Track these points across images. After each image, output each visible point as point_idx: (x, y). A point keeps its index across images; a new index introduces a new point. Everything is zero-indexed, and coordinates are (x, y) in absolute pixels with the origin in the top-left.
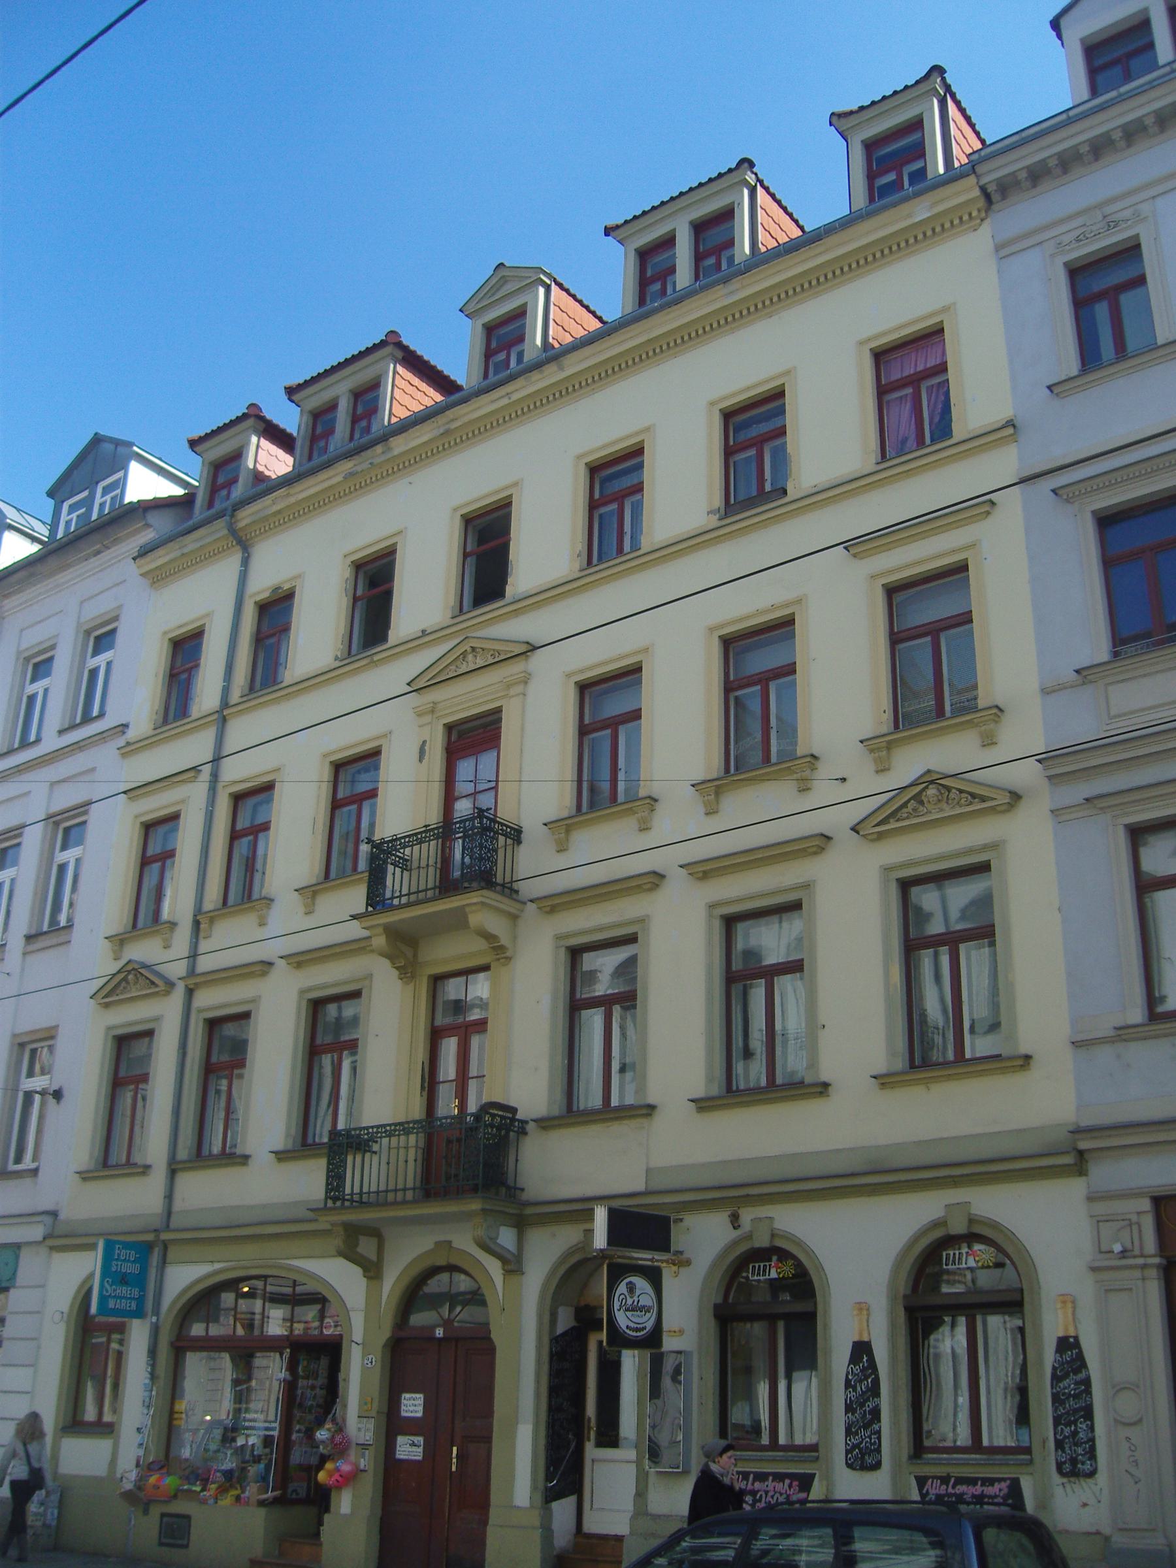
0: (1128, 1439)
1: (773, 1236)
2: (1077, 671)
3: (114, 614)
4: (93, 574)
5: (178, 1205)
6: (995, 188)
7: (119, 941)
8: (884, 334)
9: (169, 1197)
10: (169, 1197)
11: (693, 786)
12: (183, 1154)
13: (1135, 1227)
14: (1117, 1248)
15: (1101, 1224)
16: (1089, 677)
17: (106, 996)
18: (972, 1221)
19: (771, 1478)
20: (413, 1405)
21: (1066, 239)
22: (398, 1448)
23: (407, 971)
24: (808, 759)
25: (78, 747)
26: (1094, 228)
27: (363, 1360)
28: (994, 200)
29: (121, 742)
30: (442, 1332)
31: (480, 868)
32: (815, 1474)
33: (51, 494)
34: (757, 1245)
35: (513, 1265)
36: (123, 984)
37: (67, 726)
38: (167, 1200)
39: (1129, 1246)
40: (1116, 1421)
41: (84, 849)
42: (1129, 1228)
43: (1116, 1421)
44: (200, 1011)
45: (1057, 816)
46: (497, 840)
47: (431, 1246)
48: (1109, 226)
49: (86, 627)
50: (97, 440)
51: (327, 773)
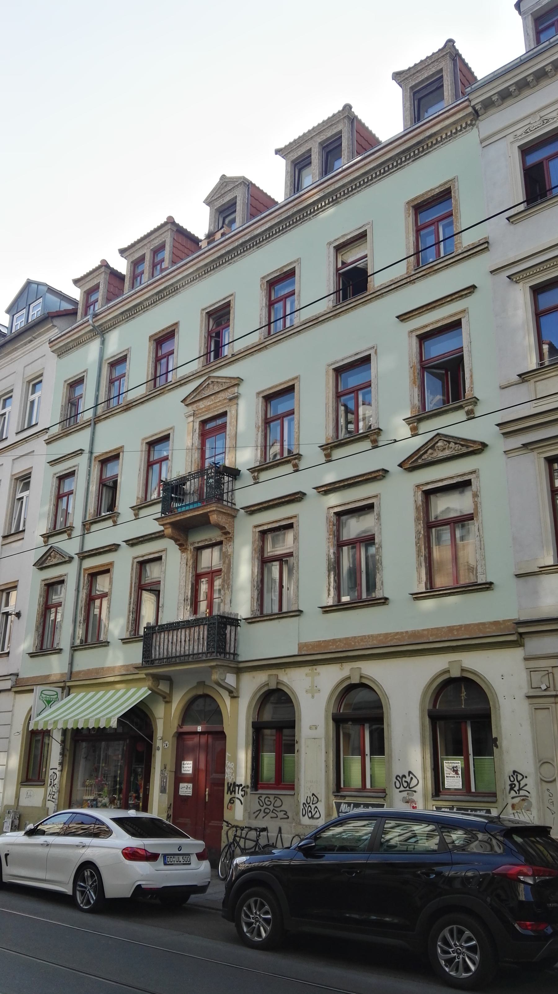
0: (548, 790)
1: (361, 677)
2: (518, 375)
3: (40, 373)
4: (30, 352)
5: (76, 669)
6: (480, 106)
7: (47, 537)
8: (277, 386)
9: (71, 664)
10: (71, 664)
11: (319, 447)
12: (78, 642)
13: (551, 675)
14: (544, 687)
15: (532, 672)
16: (525, 379)
17: (40, 565)
18: (463, 670)
19: (362, 806)
20: (188, 767)
21: (519, 133)
22: (180, 790)
23: (182, 547)
24: (377, 431)
25: (25, 440)
26: (535, 124)
27: (163, 745)
28: (480, 114)
29: (46, 437)
30: (200, 729)
31: (215, 493)
32: (384, 804)
33: (8, 311)
34: (353, 682)
35: (234, 694)
36: (49, 558)
37: (20, 430)
38: (70, 665)
39: (548, 685)
40: (541, 779)
41: (30, 492)
42: (547, 675)
43: (541, 779)
44: (85, 570)
45: (507, 454)
46: (224, 478)
47: (195, 684)
48: (544, 122)
49: (28, 379)
50: (29, 283)
51: (144, 447)
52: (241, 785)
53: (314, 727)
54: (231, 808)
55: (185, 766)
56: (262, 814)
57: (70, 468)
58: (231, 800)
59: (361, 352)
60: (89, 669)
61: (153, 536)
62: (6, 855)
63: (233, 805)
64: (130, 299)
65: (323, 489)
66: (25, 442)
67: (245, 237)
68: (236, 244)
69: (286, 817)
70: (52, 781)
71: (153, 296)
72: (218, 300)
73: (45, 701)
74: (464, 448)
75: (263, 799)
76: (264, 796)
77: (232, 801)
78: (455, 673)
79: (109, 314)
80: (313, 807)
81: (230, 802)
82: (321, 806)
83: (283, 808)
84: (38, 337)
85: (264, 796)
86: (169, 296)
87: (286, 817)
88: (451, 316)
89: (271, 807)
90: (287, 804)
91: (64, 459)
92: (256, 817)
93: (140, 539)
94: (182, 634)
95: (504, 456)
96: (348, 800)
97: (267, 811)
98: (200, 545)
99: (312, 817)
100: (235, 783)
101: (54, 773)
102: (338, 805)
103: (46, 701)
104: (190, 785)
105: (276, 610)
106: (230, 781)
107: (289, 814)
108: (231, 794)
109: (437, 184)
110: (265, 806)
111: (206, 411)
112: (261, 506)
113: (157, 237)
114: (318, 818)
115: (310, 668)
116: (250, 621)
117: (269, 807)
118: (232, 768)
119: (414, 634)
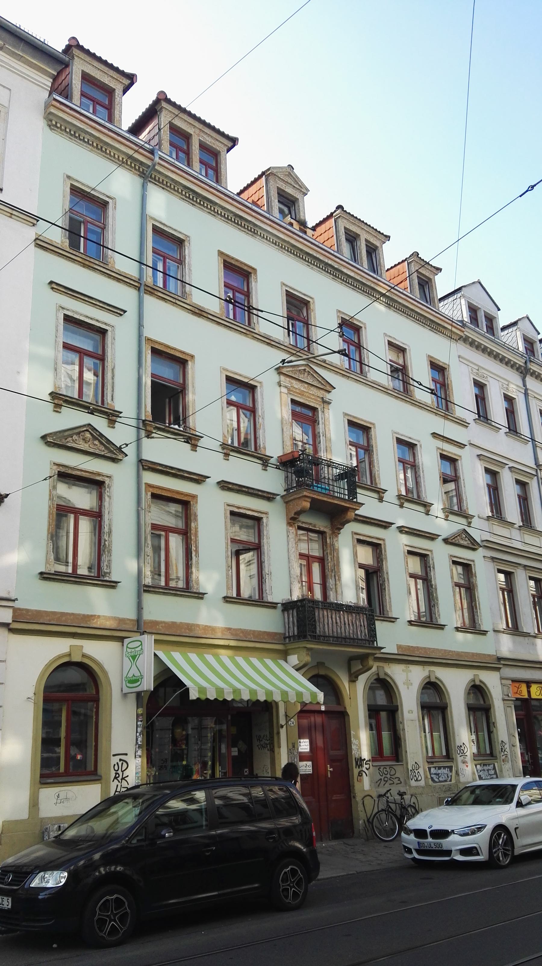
18: (84, 656)
52: (365, 759)
53: (411, 712)
54: (361, 779)
55: (301, 744)
56: (383, 782)
57: (97, 321)
58: (359, 773)
59: (413, 439)
60: (175, 623)
61: (260, 493)
62: (516, 829)
63: (361, 778)
64: (230, 201)
65: (407, 530)
66: (9, 215)
67: (336, 264)
68: (326, 260)
69: (399, 782)
70: (120, 772)
71: (232, 212)
72: (299, 290)
73: (130, 658)
74: (106, 451)
75: (381, 770)
76: (382, 768)
77: (360, 774)
78: (77, 658)
79: (173, 171)
80: (416, 772)
81: (359, 775)
82: (421, 771)
83: (396, 776)
84: (5, 52)
85: (382, 768)
86: (244, 230)
87: (399, 782)
88: (455, 454)
89: (388, 776)
90: (399, 772)
91: (86, 299)
92: (379, 785)
93: (244, 489)
94: (346, 617)
95: (483, 558)
96: (435, 765)
97: (386, 779)
98: (304, 525)
99: (417, 780)
100: (361, 758)
101: (120, 760)
102: (430, 769)
103: (132, 656)
104: (309, 763)
105: (181, 584)
106: (357, 756)
107: (402, 780)
108: (359, 768)
109: (443, 361)
110: (384, 776)
111: (300, 394)
112: (365, 519)
113: (212, 137)
114: (420, 780)
115: (405, 665)
116: (45, 576)
117: (387, 776)
118: (357, 745)
119: (458, 654)
